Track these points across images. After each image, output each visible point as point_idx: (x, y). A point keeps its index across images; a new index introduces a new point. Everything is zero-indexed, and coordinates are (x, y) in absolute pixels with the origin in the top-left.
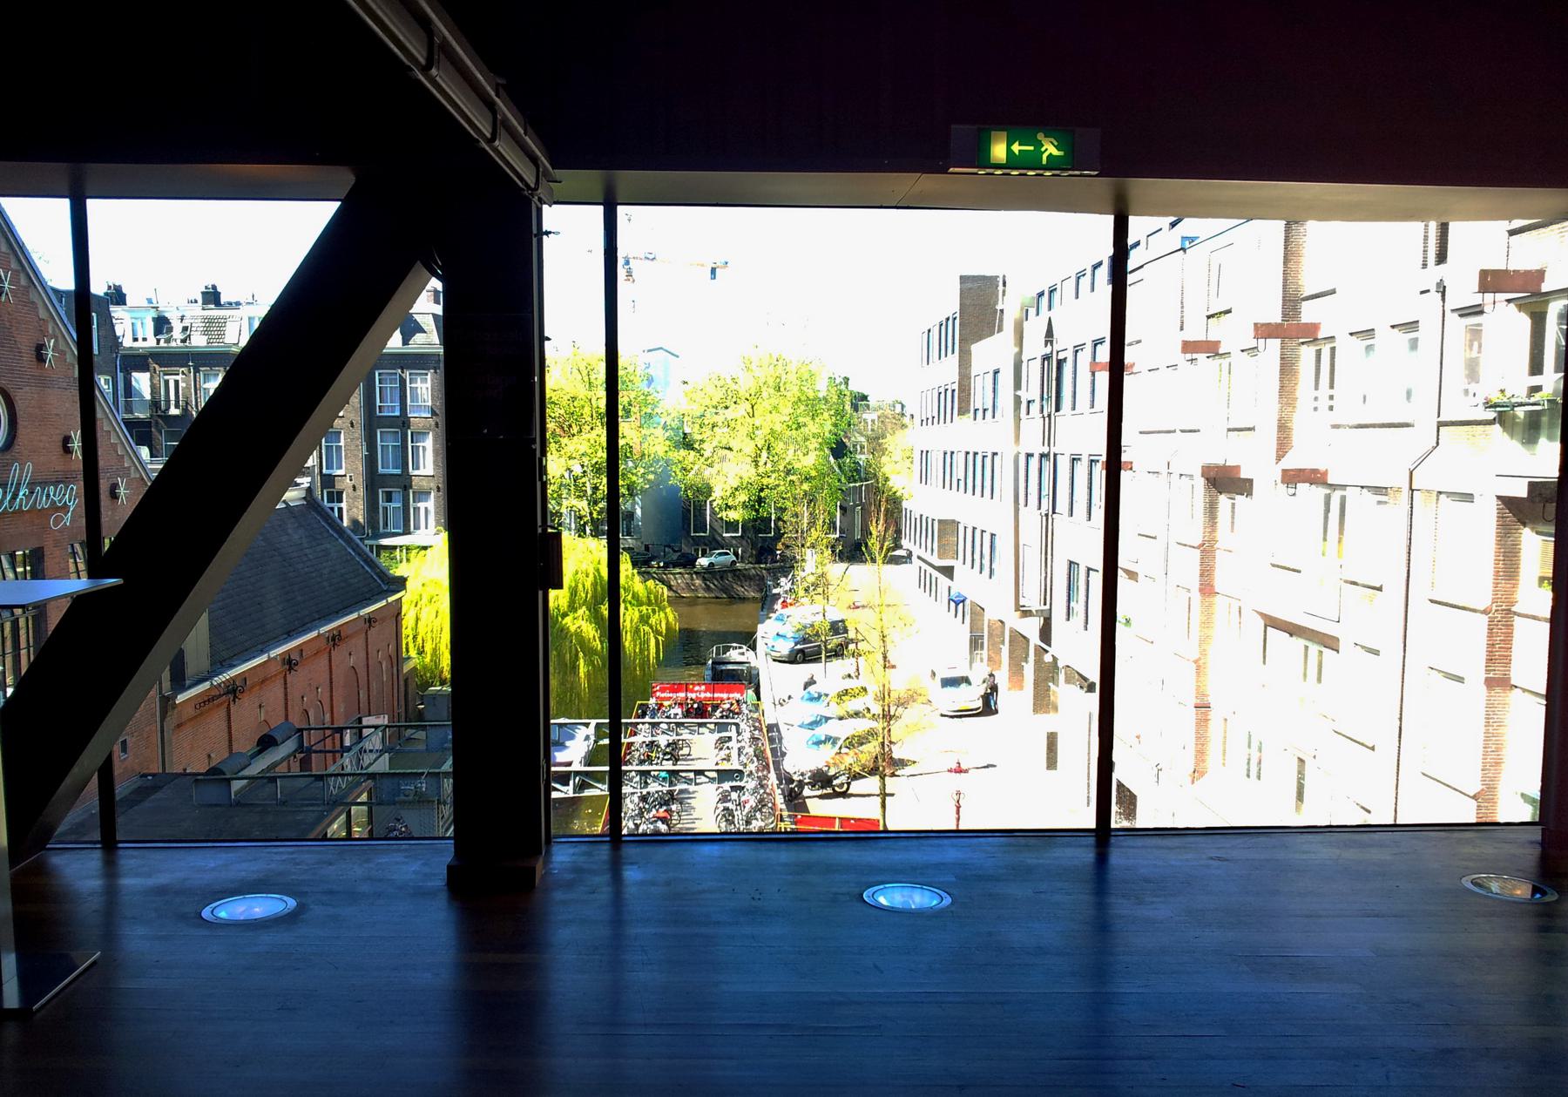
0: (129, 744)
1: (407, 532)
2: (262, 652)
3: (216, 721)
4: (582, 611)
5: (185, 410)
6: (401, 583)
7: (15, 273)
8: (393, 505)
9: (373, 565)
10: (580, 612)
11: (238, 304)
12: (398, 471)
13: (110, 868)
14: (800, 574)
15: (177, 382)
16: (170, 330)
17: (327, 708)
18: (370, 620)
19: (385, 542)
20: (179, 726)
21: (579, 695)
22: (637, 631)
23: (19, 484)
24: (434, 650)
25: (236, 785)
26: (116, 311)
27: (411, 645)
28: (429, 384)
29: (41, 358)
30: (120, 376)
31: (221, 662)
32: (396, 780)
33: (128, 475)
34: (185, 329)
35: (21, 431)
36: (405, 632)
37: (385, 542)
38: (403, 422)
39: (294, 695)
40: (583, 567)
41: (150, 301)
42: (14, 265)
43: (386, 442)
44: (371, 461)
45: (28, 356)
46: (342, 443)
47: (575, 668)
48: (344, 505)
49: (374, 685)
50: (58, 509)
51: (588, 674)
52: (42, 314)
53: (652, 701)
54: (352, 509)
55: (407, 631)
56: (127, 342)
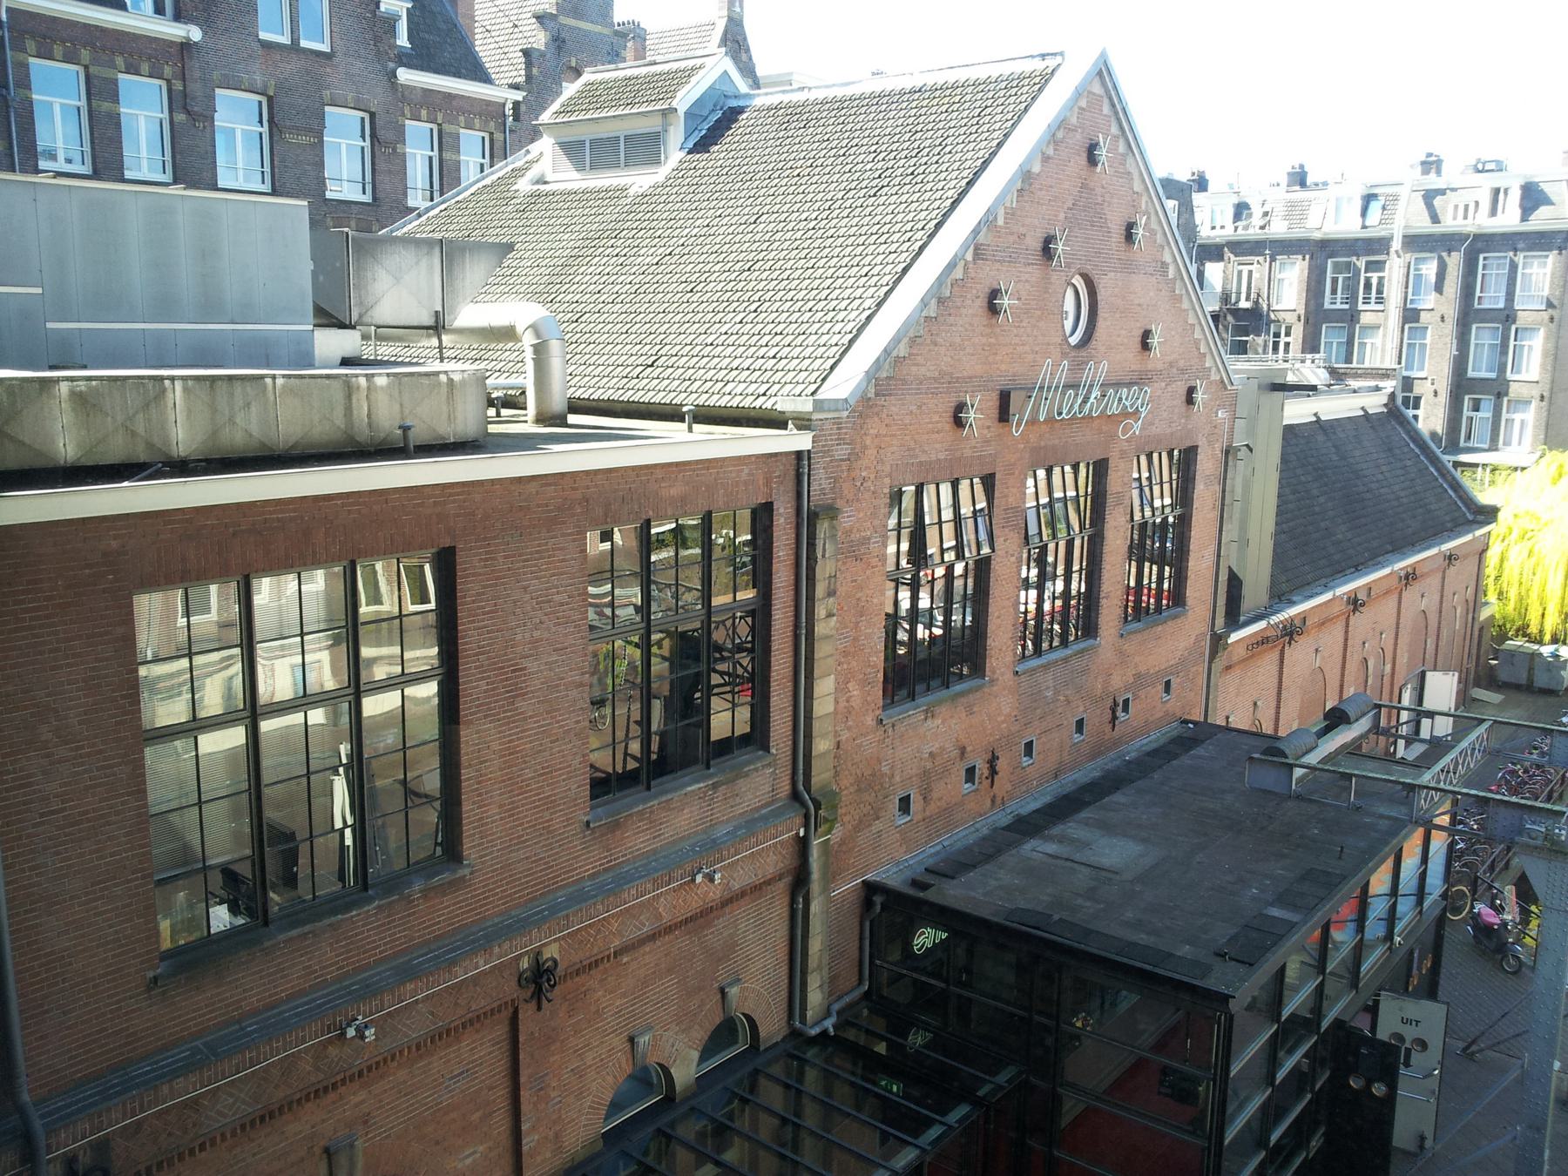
0: (1173, 685)
1: (1493, 447)
2: (1326, 588)
3: (1268, 662)
5: (1256, 302)
6: (1489, 514)
7: (1116, 137)
8: (1480, 414)
9: (1457, 486)
11: (1325, 184)
12: (1493, 375)
15: (1250, 272)
16: (1250, 215)
18: (1450, 558)
19: (1464, 458)
20: (1228, 668)
23: (1091, 386)
25: (1298, 772)
26: (1198, 198)
28: (1549, 269)
29: (1129, 237)
31: (1280, 595)
34: (1266, 214)
35: (1101, 325)
36: (1488, 571)
37: (1464, 458)
38: (1507, 317)
39: (1355, 642)
41: (1231, 186)
42: (1114, 130)
43: (1482, 338)
46: (1428, 341)
48: (1420, 412)
49: (1445, 633)
52: (1137, 187)
54: (1430, 418)
55: (1490, 570)
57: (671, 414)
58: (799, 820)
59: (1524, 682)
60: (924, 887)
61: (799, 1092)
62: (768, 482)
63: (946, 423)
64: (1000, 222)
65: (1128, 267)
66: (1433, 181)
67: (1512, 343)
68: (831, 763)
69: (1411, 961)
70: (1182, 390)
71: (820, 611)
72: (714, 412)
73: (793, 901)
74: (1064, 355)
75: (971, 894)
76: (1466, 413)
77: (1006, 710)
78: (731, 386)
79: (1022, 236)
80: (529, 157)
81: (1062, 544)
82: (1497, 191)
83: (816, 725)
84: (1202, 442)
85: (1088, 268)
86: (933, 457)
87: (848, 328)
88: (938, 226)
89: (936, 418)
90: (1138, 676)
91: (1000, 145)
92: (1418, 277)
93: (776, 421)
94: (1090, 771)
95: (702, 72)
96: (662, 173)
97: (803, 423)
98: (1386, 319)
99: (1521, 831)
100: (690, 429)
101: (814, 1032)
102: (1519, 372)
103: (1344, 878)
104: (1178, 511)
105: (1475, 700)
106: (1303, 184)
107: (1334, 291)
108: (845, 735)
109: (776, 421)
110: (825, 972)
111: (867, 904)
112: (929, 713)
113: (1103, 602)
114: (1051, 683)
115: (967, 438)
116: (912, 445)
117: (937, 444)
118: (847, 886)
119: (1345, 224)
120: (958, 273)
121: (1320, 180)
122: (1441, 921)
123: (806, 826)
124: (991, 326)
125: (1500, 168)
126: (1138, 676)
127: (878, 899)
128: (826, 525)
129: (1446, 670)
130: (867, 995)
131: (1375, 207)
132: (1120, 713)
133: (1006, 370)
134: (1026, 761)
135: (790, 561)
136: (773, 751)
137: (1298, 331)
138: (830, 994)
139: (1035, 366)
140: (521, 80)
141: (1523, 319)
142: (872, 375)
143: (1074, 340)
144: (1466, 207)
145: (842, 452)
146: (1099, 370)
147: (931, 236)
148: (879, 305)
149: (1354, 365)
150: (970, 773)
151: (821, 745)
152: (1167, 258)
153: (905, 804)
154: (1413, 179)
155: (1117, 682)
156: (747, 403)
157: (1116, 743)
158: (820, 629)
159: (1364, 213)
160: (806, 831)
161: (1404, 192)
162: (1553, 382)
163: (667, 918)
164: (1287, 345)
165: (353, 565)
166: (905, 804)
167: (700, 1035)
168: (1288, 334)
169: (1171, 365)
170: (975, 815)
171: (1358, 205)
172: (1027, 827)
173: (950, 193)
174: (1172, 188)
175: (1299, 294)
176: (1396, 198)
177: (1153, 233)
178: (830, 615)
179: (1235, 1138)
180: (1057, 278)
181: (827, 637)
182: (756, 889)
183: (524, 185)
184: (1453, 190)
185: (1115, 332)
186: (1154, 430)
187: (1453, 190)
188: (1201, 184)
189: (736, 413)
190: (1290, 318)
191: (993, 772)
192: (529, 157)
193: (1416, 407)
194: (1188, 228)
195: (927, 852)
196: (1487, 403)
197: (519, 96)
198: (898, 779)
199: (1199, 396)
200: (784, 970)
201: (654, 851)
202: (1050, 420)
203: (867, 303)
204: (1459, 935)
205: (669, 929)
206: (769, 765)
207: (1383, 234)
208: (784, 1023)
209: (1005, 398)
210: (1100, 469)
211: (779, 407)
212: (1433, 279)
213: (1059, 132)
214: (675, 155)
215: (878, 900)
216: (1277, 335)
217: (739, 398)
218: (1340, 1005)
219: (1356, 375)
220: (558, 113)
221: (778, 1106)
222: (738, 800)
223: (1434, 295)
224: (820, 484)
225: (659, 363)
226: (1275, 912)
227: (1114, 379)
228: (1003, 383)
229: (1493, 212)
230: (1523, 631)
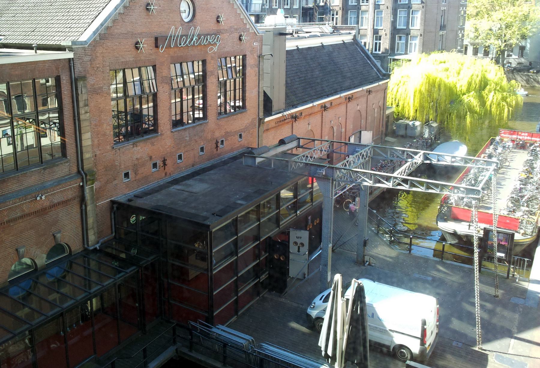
0: (243, 135)
4: (472, 93)
10: (471, 93)
12: (405, 27)
14: (135, 148)
17: (343, 126)
20: (267, 130)
22: (499, 104)
23: (193, 35)
24: (403, 105)
25: (258, 160)
33: (249, 31)
37: (396, 57)
43: (401, 14)
44: (394, 23)
46: (383, 16)
49: (369, 118)
50: (212, 45)
51: (471, 123)
53: (498, 138)
57: (29, 47)
58: (79, 180)
61: (89, 269)
67: (411, 16)
70: (237, 36)
71: (82, 111)
72: (53, 47)
73: (81, 207)
75: (146, 203)
76: (397, 41)
77: (169, 144)
83: (84, 149)
84: (248, 54)
86: (128, 60)
89: (127, 47)
90: (227, 133)
94: (208, 164)
98: (369, 8)
100: (36, 52)
101: (91, 248)
102: (413, 26)
105: (386, 141)
108: (98, 153)
110: (96, 229)
111: (112, 208)
112: (134, 145)
114: (188, 135)
116: (118, 56)
118: (104, 202)
123: (83, 182)
126: (227, 133)
127: (115, 206)
128: (81, 82)
130: (115, 237)
132: (219, 144)
133: (157, 30)
134: (179, 161)
136: (69, 158)
137: (340, 13)
138: (99, 237)
141: (414, 7)
149: (349, 25)
150: (155, 165)
151: (86, 156)
153: (127, 175)
155: (217, 134)
157: (219, 155)
158: (82, 117)
160: (83, 183)
162: (424, 30)
163: (27, 211)
164: (337, 18)
166: (127, 175)
167: (46, 249)
168: (337, 14)
169: (231, 27)
170: (158, 178)
172: (176, 182)
178: (86, 113)
179: (242, 275)
181: (85, 120)
182: (65, 203)
189: (56, 47)
190: (337, 9)
191: (165, 164)
193: (380, 40)
195: (131, 193)
196: (404, 38)
198: (123, 167)
200: (80, 229)
201: (21, 190)
205: (29, 215)
206: (67, 162)
208: (81, 246)
216: (333, 15)
221: (82, 274)
222: (55, 174)
224: (78, 69)
228: (156, 35)
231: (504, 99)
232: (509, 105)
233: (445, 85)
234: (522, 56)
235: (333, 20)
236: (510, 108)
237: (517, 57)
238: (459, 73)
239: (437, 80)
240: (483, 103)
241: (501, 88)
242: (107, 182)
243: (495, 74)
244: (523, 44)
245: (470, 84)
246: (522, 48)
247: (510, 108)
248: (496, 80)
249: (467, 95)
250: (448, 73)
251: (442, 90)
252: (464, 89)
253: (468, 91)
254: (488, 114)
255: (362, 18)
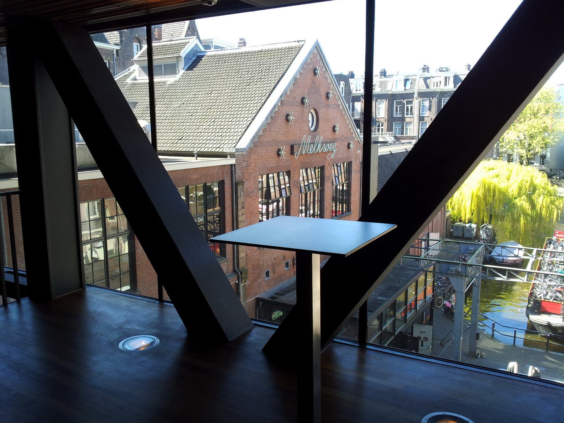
11: (392, 75)
13: (362, 360)
21: (520, 233)
26: (351, 80)
27: (449, 206)
29: (328, 97)
30: (351, 104)
32: (448, 265)
35: (320, 124)
40: (525, 179)
42: (321, 64)
45: (324, 97)
47: (519, 221)
51: (525, 224)
52: (329, 81)
53: (554, 238)
56: (354, 92)
57: (191, 154)
58: (236, 278)
59: (461, 236)
60: (275, 298)
62: (223, 174)
63: (275, 155)
64: (288, 94)
65: (328, 106)
66: (426, 75)
68: (245, 260)
69: (423, 315)
71: (240, 213)
74: (309, 134)
78: (207, 145)
79: (295, 98)
80: (130, 71)
81: (312, 192)
82: (446, 78)
84: (353, 160)
85: (315, 107)
87: (244, 126)
88: (269, 95)
89: (272, 154)
91: (287, 70)
92: (423, 106)
93: (223, 155)
95: (189, 44)
96: (178, 77)
97: (232, 155)
99: (449, 270)
100: (197, 159)
103: (400, 288)
104: (347, 182)
106: (385, 76)
107: (397, 111)
109: (223, 155)
113: (325, 210)
115: (282, 159)
117: (273, 162)
119: (399, 89)
120: (277, 109)
121: (390, 74)
122: (432, 303)
123: (238, 280)
124: (287, 125)
125: (447, 70)
127: (261, 303)
128: (241, 186)
129: (435, 232)
131: (408, 83)
133: (292, 139)
135: (230, 198)
137: (385, 124)
139: (301, 137)
140: (118, 42)
142: (253, 141)
143: (312, 129)
144: (437, 83)
145: (244, 164)
146: (320, 138)
147: (267, 98)
148: (253, 119)
150: (287, 264)
152: (340, 103)
153: (267, 274)
154: (419, 74)
156: (213, 150)
159: (405, 85)
161: (417, 78)
164: (382, 129)
165: (103, 200)
166: (267, 274)
168: (382, 126)
171: (403, 82)
173: (272, 85)
174: (340, 77)
175: (385, 112)
176: (415, 80)
177: (335, 95)
178: (243, 214)
180: (306, 110)
183: (129, 81)
184: (433, 77)
185: (325, 126)
186: (339, 157)
187: (433, 77)
188: (352, 75)
190: (383, 120)
192: (130, 71)
194: (348, 91)
195: (276, 288)
197: (118, 47)
198: (265, 266)
199: (351, 146)
202: (306, 154)
203: (249, 119)
204: (439, 311)
207: (411, 92)
209: (292, 147)
210: (322, 169)
211: (224, 151)
212: (428, 107)
213: (305, 65)
214: (182, 72)
215: (261, 303)
216: (379, 126)
217: (210, 149)
218: (401, 327)
219: (403, 139)
220: (140, 57)
223: (428, 112)
224: (238, 174)
225: (183, 138)
226: (379, 298)
227: (325, 141)
228: (291, 143)
229: (446, 85)
230: (461, 221)
231: (552, 202)
232: (558, 208)
233: (500, 190)
234: (543, 164)
235: (379, 131)
236: (559, 211)
237: (539, 165)
238: (508, 179)
239: (492, 186)
240: (533, 206)
241: (547, 192)
242: (253, 281)
243: (541, 180)
244: (544, 153)
245: (520, 189)
246: (543, 157)
247: (559, 211)
248: (543, 185)
249: (519, 199)
250: (498, 178)
251: (497, 193)
252: (515, 193)
253: (519, 195)
254: (539, 218)
255: (407, 129)
